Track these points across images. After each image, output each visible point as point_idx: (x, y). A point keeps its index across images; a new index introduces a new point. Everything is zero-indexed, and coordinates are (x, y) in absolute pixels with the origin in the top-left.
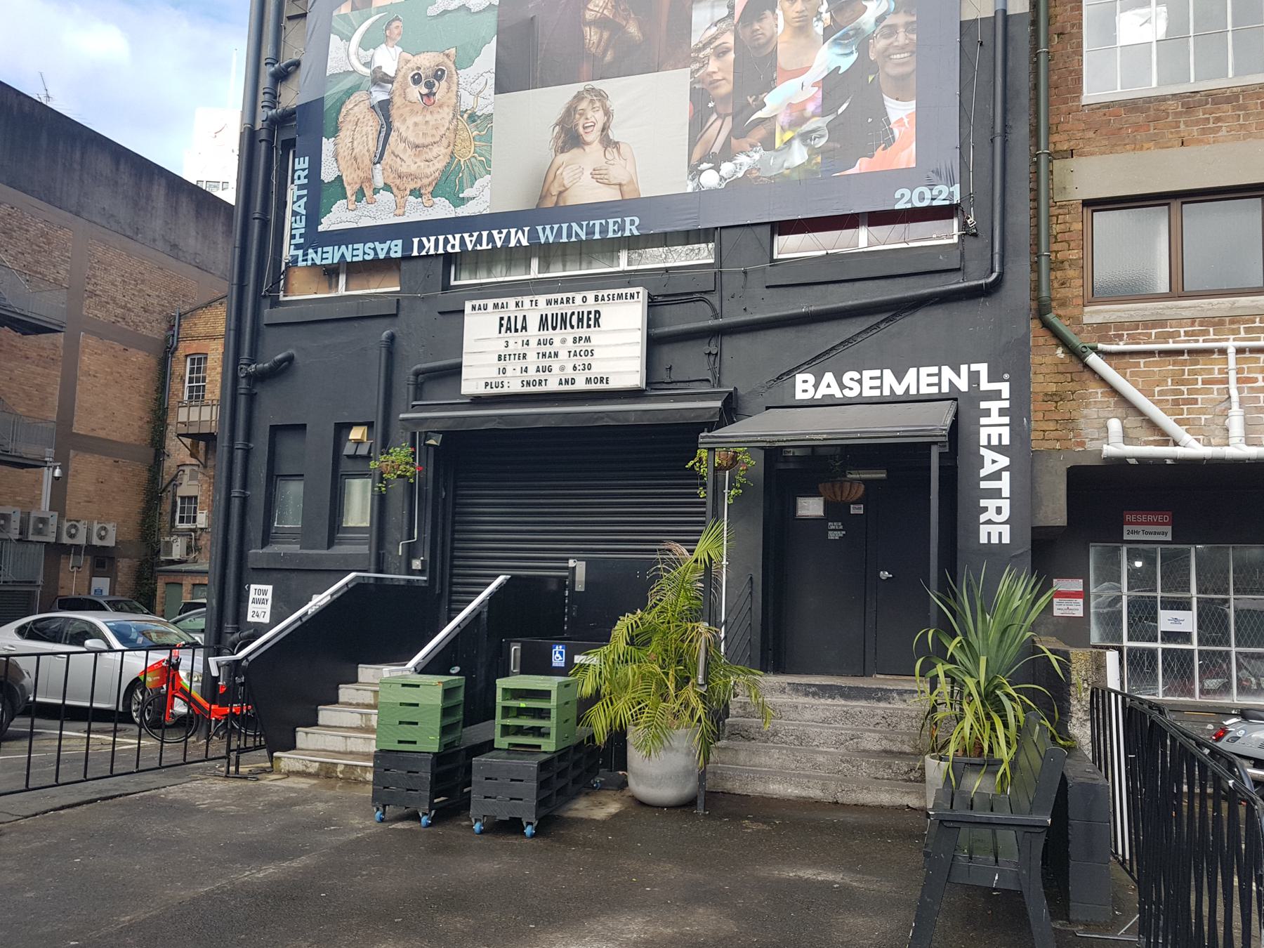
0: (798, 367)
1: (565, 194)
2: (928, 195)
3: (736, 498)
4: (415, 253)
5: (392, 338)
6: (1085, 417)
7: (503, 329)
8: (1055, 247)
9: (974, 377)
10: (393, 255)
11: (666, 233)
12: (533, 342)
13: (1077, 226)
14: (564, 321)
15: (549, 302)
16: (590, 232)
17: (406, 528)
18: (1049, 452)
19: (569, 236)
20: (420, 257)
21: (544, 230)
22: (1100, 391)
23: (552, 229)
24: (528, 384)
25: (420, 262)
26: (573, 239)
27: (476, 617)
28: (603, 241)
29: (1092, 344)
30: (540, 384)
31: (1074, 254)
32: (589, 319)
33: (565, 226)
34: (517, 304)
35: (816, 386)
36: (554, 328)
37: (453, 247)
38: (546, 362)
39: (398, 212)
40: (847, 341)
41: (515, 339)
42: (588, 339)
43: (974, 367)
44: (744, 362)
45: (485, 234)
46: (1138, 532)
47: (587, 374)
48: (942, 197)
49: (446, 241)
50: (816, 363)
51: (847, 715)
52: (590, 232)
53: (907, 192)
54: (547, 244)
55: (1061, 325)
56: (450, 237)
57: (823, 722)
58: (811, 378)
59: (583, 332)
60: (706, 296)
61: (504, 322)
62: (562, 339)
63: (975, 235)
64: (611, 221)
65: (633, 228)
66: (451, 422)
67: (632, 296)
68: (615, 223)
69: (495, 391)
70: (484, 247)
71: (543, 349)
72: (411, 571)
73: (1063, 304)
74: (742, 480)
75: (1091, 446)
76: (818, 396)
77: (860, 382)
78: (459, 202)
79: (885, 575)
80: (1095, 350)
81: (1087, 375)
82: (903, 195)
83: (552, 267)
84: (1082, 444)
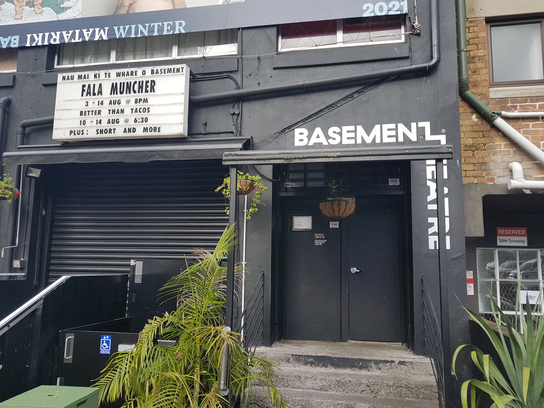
0: (296, 124)
1: (134, 5)
2: (385, 8)
3: (253, 215)
4: (28, 45)
5: (8, 103)
6: (493, 161)
7: (85, 93)
8: (469, 48)
9: (421, 132)
10: (12, 46)
11: (205, 32)
12: (106, 103)
13: (483, 34)
14: (129, 87)
15: (118, 75)
16: (151, 30)
17: (10, 237)
18: (470, 185)
19: (136, 33)
20: (31, 47)
21: (119, 29)
22: (503, 144)
23: (124, 29)
24: (102, 132)
25: (32, 52)
26: (139, 35)
27: (32, 315)
28: (161, 37)
29: (499, 112)
30: (110, 132)
31: (481, 53)
32: (147, 86)
33: (133, 27)
34: (95, 76)
35: (309, 137)
36: (121, 93)
37: (55, 40)
38: (115, 116)
39: (17, 17)
40: (331, 106)
41: (93, 101)
42: (146, 101)
43: (421, 124)
44: (257, 119)
45: (77, 32)
46: (506, 241)
47: (145, 125)
48: (396, 9)
49: (50, 37)
50: (309, 121)
51: (340, 384)
52: (151, 30)
53: (371, 5)
54: (120, 39)
55: (477, 99)
56: (53, 34)
57: (321, 389)
58: (305, 131)
59: (143, 95)
60: (232, 75)
61: (86, 89)
62: (128, 101)
63: (418, 35)
64: (166, 24)
65: (181, 28)
66: (41, 158)
67: (178, 70)
68: (168, 25)
69: (77, 137)
70: (77, 40)
71: (113, 107)
72: (11, 269)
73: (475, 85)
74: (258, 201)
75: (499, 181)
76: (311, 144)
77: (340, 134)
78: (59, 10)
79: (354, 270)
80: (499, 115)
81: (493, 133)
82: (368, 8)
83: (126, 58)
84: (492, 180)
